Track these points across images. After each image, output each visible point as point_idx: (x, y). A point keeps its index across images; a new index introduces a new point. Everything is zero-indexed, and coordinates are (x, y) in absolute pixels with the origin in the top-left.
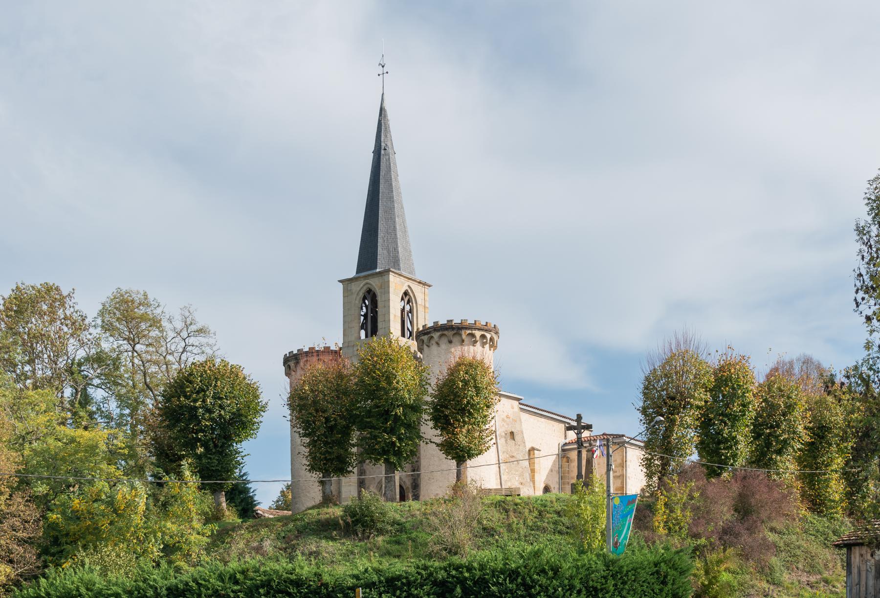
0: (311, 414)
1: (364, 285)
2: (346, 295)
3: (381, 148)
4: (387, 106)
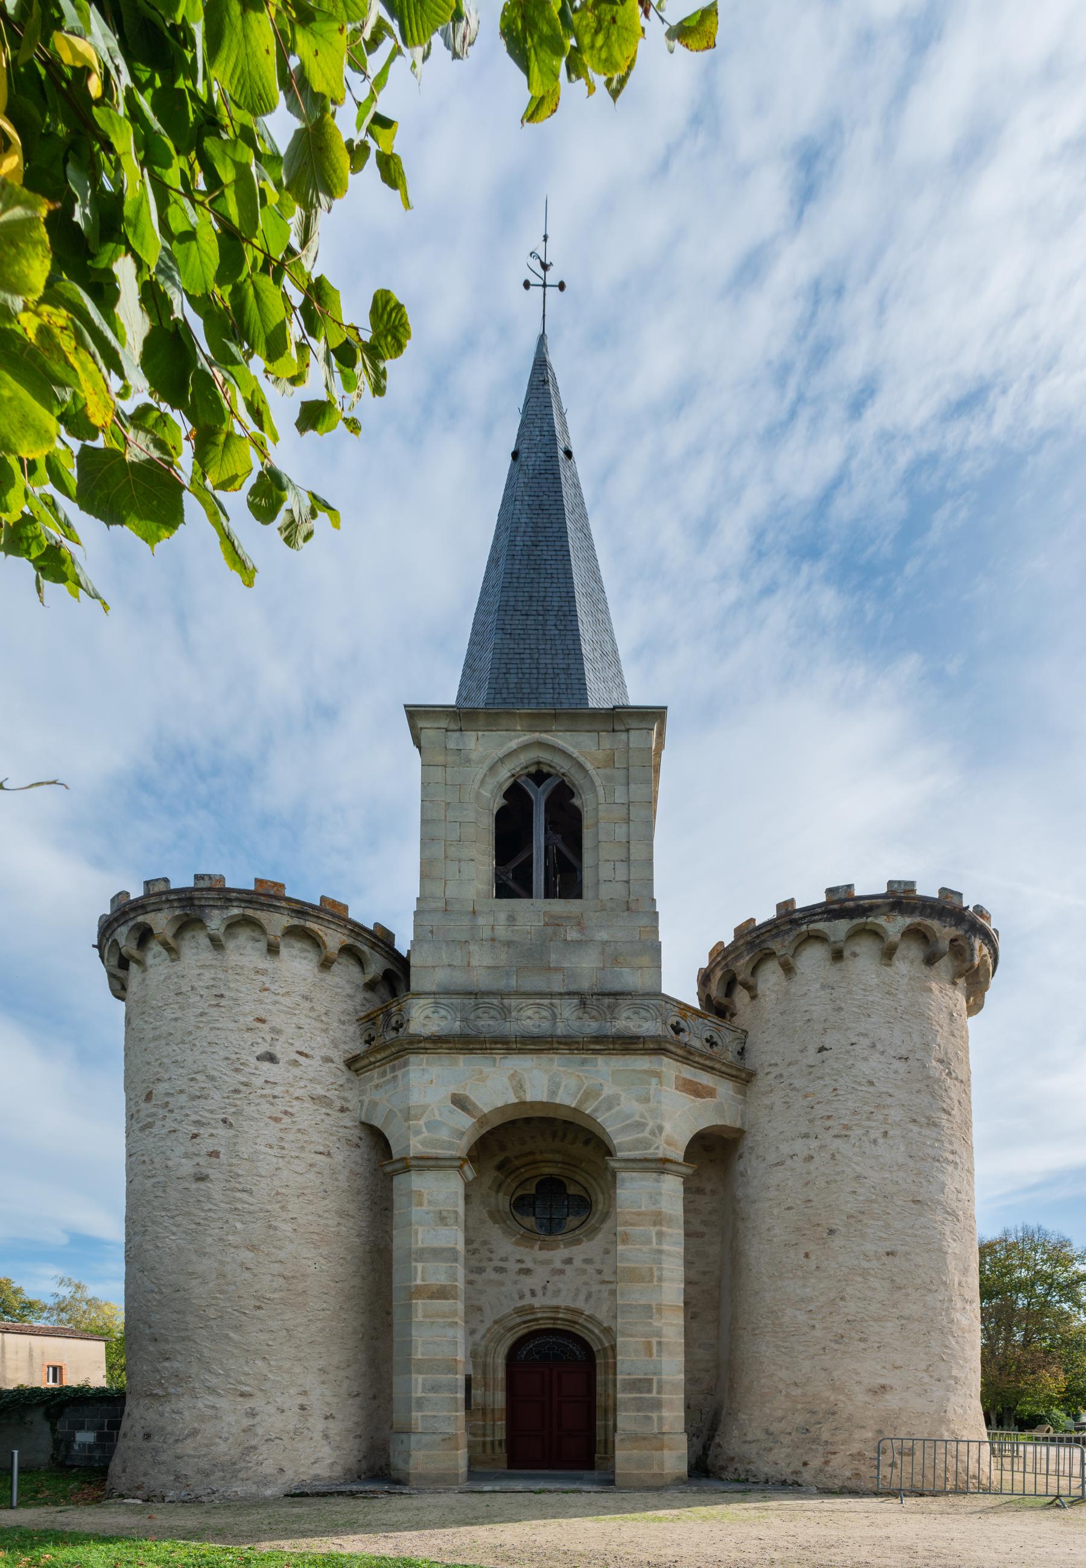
1: (525, 747)
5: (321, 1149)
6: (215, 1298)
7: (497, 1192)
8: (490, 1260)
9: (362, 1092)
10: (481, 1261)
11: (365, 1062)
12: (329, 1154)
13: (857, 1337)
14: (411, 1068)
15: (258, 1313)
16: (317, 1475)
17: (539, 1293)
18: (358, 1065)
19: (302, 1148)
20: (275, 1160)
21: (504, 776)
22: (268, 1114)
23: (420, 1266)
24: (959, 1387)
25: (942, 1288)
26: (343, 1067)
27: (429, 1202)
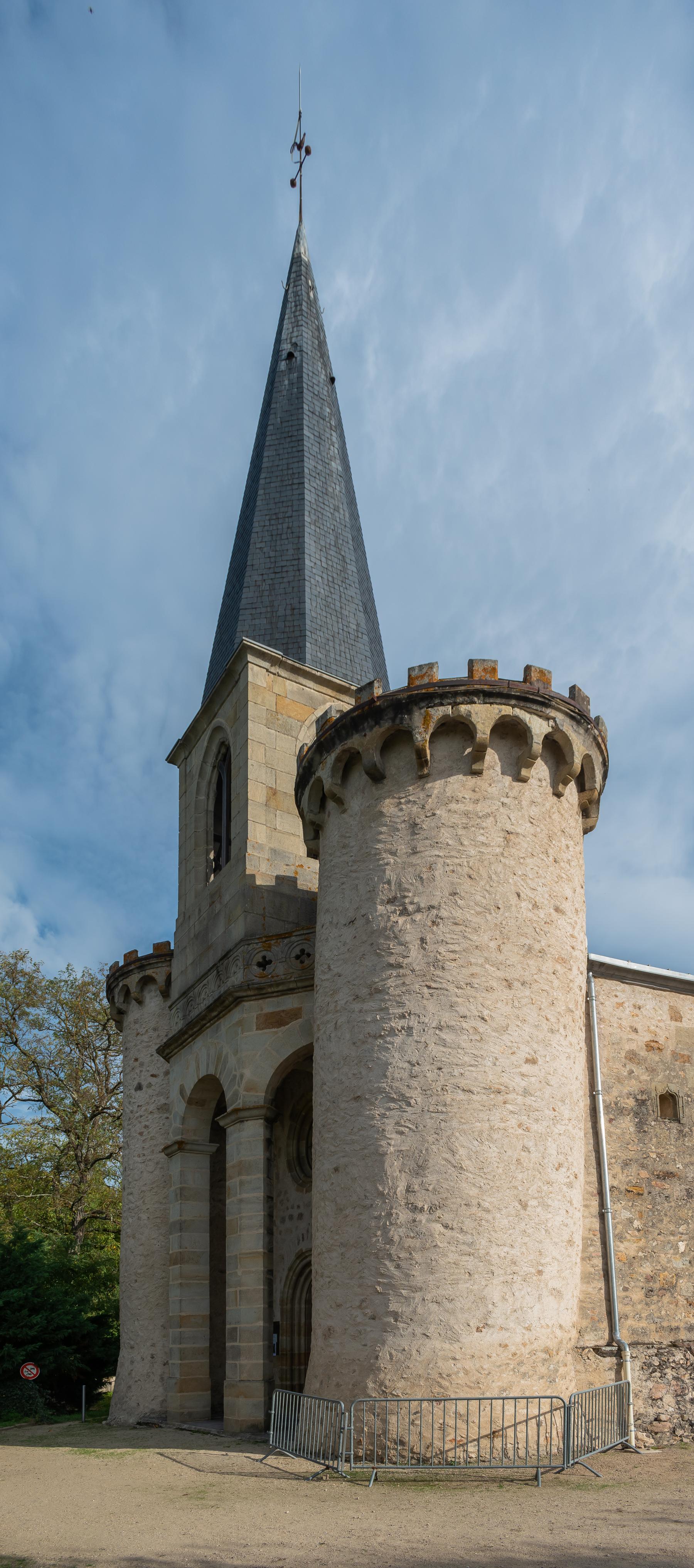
16: (153, 1409)
24: (401, 1325)
25: (378, 1202)
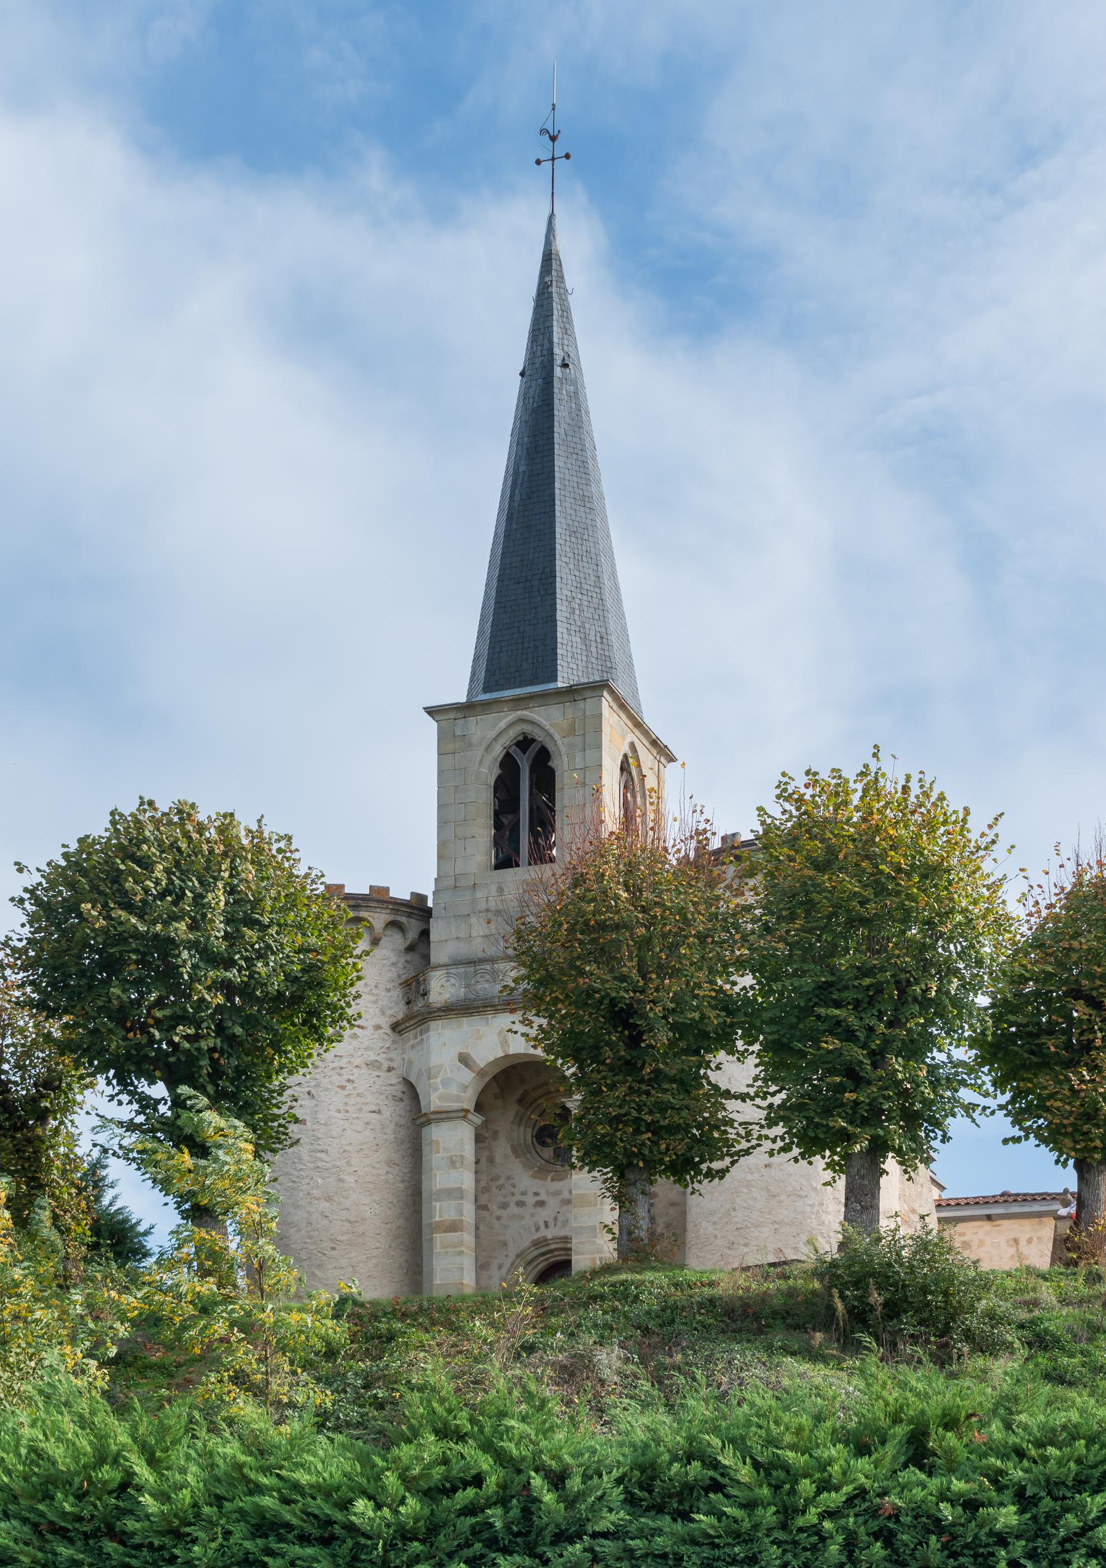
0: (623, 978)
1: (512, 725)
2: (450, 747)
3: (553, 360)
4: (561, 245)
5: (374, 1108)
6: (306, 1243)
7: (519, 1125)
8: (513, 1194)
9: (404, 1051)
10: (505, 1196)
11: (403, 1026)
12: (379, 1112)
13: (742, 1242)
14: (431, 1033)
15: (334, 1253)
17: (551, 1224)
18: (400, 1028)
19: (361, 1110)
20: (342, 1122)
21: (498, 751)
22: (337, 1084)
23: (437, 1205)
25: (812, 1193)
26: (389, 1031)
27: (444, 1149)
